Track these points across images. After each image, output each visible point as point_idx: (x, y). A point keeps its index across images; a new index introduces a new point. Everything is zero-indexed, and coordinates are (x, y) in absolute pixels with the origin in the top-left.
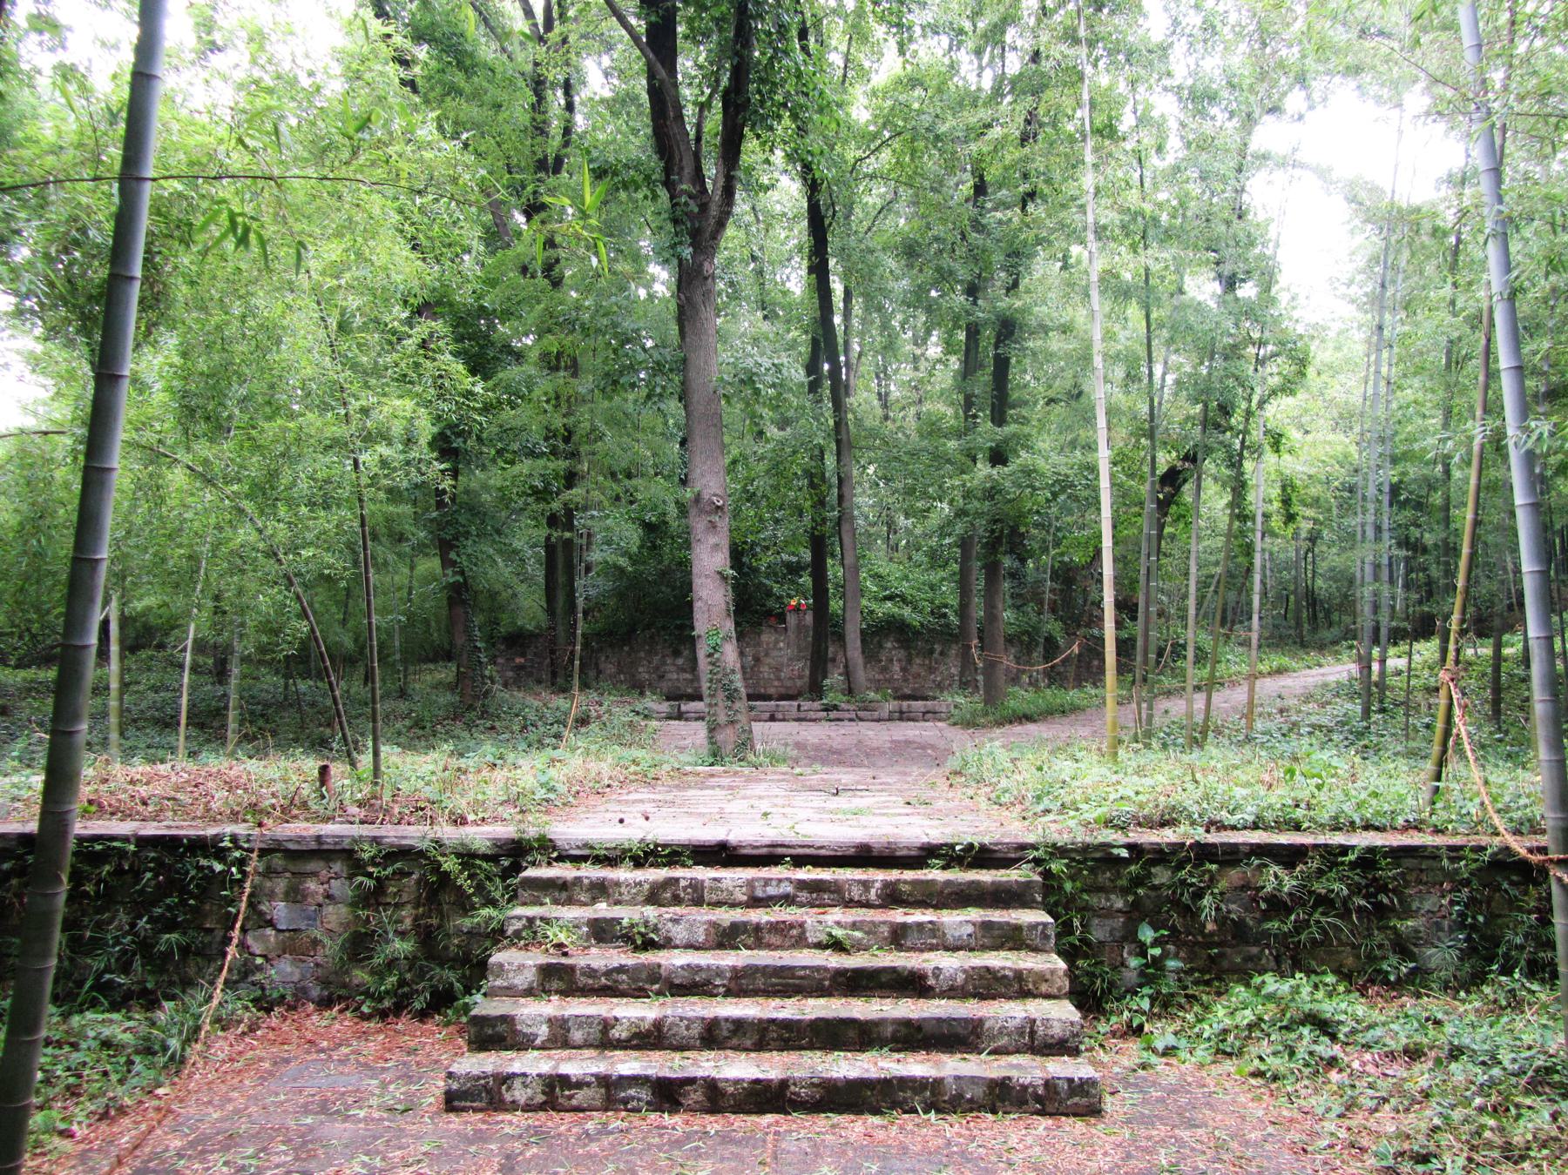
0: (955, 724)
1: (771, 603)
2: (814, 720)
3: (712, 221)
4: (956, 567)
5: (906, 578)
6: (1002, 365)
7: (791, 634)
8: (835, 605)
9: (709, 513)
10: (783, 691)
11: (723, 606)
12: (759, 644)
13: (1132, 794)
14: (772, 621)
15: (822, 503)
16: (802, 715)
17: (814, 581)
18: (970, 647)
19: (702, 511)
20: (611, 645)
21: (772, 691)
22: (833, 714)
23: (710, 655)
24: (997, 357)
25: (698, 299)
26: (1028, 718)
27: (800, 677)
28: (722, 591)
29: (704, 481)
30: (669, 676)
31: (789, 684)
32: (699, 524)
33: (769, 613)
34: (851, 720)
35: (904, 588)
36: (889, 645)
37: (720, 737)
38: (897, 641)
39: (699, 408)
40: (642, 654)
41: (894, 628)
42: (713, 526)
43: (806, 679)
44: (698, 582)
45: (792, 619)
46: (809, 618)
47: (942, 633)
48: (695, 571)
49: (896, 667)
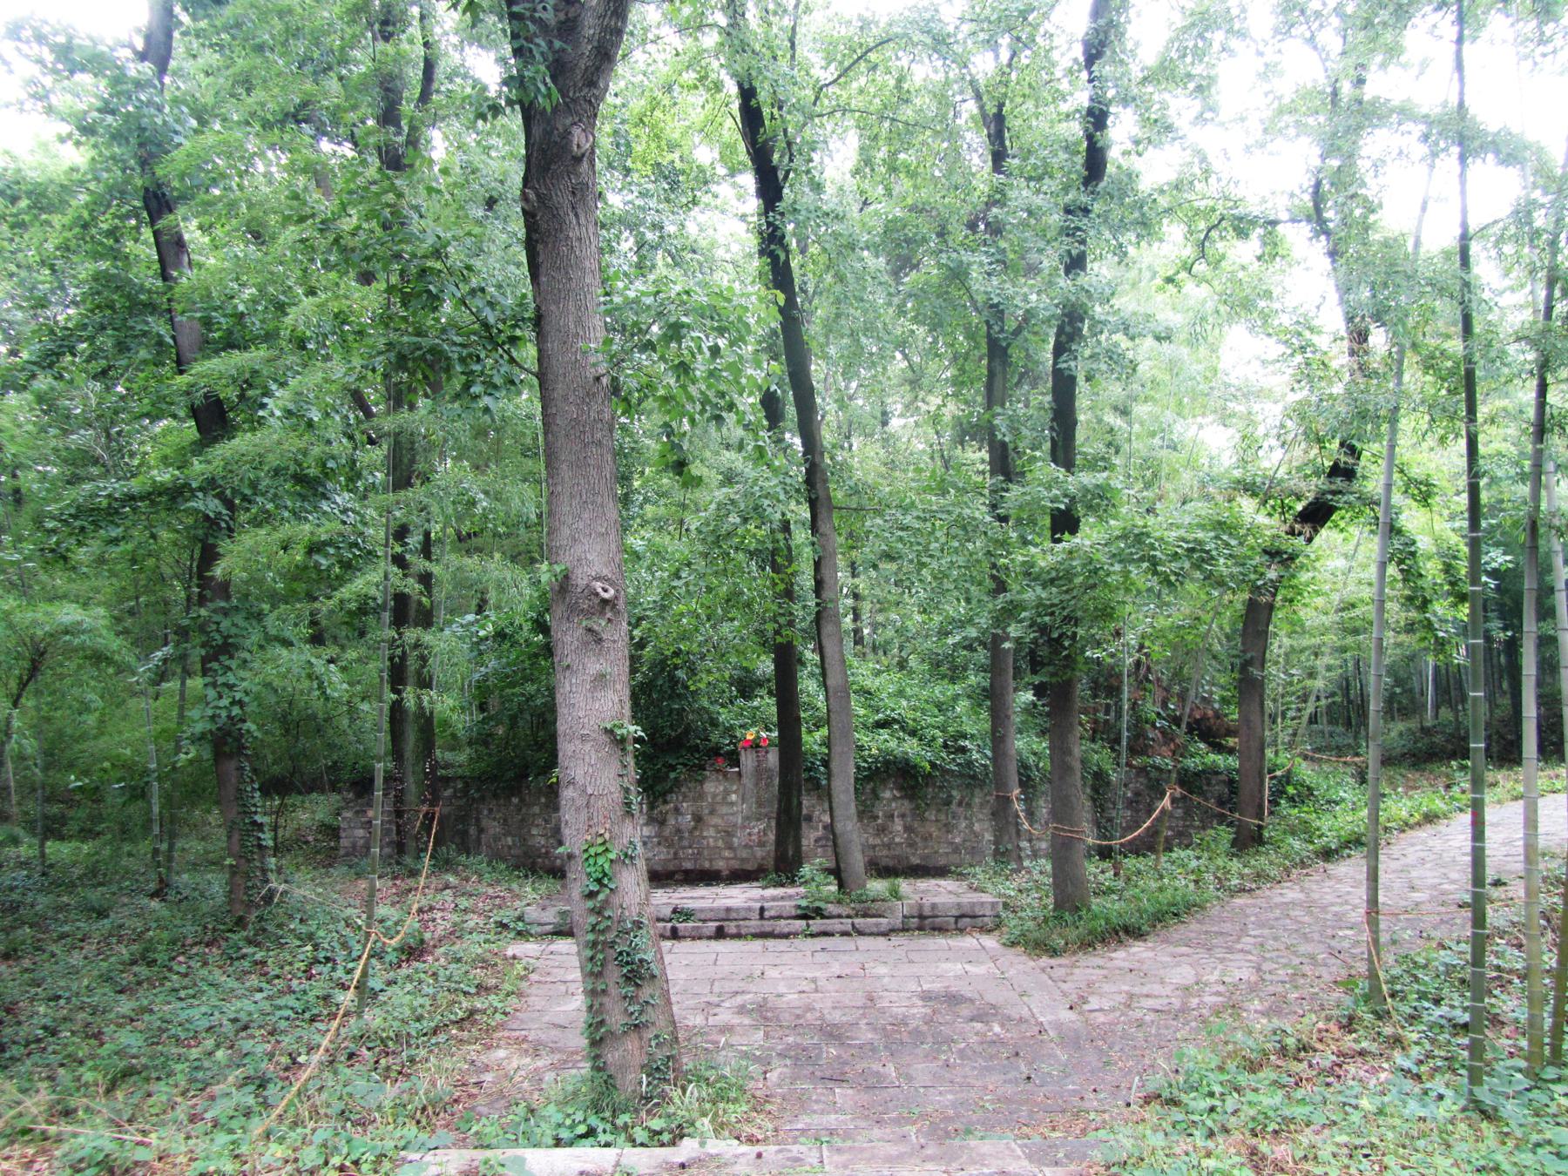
0: (1013, 944)
1: (715, 737)
2: (786, 936)
3: (587, 48)
4: (1365, 812)
5: (900, 693)
6: (1064, 388)
7: (748, 781)
8: (812, 740)
9: (588, 614)
10: (736, 865)
11: (618, 796)
12: (701, 796)
14: (721, 763)
15: (789, 594)
16: (767, 926)
17: (780, 705)
18: (1008, 800)
19: (574, 610)
20: (495, 796)
21: (720, 865)
22: (817, 924)
23: (591, 895)
24: (1057, 373)
25: (562, 198)
26: (1130, 932)
27: (761, 844)
28: (615, 767)
29: (578, 550)
31: (744, 854)
32: (568, 637)
33: (715, 752)
34: (845, 934)
35: (902, 708)
36: (887, 794)
37: (612, 1056)
38: (901, 789)
39: (568, 411)
40: (536, 809)
41: (901, 773)
42: (595, 637)
43: (771, 847)
44: (566, 748)
45: (748, 760)
46: (773, 758)
47: (961, 775)
48: (562, 727)
49: (898, 826)
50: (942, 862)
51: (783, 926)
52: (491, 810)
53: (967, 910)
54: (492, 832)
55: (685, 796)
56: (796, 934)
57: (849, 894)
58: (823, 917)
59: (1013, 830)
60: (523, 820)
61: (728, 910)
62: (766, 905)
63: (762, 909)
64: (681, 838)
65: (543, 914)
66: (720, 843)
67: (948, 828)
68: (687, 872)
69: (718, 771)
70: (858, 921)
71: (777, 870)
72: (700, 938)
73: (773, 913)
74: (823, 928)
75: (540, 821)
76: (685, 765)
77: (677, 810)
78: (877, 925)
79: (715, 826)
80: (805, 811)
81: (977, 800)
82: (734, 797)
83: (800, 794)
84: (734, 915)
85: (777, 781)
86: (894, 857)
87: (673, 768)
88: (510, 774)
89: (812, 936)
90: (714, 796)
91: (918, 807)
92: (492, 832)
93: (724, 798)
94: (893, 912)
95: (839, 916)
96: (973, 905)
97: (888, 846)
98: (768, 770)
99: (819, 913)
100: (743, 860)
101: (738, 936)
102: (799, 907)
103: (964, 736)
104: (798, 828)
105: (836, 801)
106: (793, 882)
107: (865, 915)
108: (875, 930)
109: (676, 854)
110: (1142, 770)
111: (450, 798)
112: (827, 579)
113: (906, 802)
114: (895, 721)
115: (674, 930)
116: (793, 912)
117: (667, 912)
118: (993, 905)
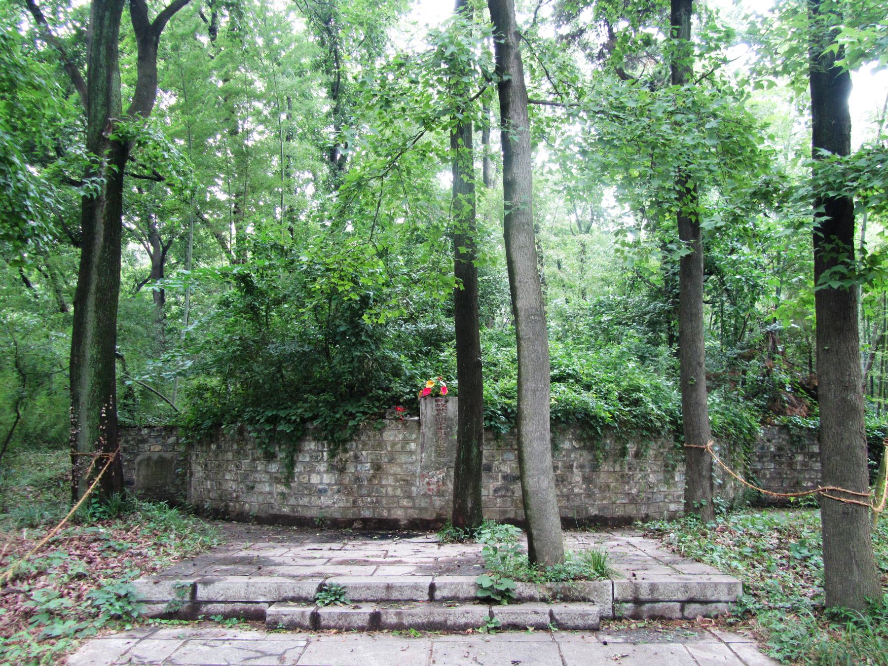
1: (397, 386)
7: (427, 431)
10: (414, 514)
12: (380, 445)
14: (400, 412)
16: (439, 613)
21: (398, 514)
22: (504, 612)
27: (440, 494)
31: (423, 503)
33: (395, 401)
34: (540, 627)
38: (580, 439)
40: (230, 456)
45: (428, 409)
46: (452, 407)
47: (637, 426)
50: (619, 512)
51: (460, 613)
53: (696, 593)
55: (364, 444)
56: (475, 627)
57: (542, 569)
58: (512, 601)
59: (706, 484)
60: (219, 466)
61: (389, 587)
62: (439, 581)
63: (432, 588)
65: (156, 589)
66: (399, 492)
67: (624, 478)
68: (365, 521)
69: (397, 419)
70: (559, 608)
71: (455, 524)
72: (348, 629)
73: (446, 593)
74: (511, 619)
75: (232, 467)
76: (364, 413)
77: (356, 457)
78: (583, 615)
79: (394, 475)
80: (484, 461)
81: (651, 452)
82: (413, 446)
83: (479, 444)
84: (395, 595)
85: (515, 9)
86: (572, 508)
87: (352, 416)
88: (208, 423)
89: (497, 629)
90: (394, 444)
91: (596, 459)
93: (403, 447)
94: (600, 594)
95: (532, 599)
96: (703, 586)
99: (507, 597)
100: (421, 509)
101: (399, 628)
102: (480, 587)
103: (638, 389)
104: (478, 478)
105: (527, 451)
106: (472, 537)
107: (566, 599)
108: (580, 622)
109: (354, 502)
110: (784, 428)
112: (519, 180)
113: (585, 453)
114: (569, 375)
115: (315, 617)
116: (472, 593)
117: (310, 588)
118: (730, 587)
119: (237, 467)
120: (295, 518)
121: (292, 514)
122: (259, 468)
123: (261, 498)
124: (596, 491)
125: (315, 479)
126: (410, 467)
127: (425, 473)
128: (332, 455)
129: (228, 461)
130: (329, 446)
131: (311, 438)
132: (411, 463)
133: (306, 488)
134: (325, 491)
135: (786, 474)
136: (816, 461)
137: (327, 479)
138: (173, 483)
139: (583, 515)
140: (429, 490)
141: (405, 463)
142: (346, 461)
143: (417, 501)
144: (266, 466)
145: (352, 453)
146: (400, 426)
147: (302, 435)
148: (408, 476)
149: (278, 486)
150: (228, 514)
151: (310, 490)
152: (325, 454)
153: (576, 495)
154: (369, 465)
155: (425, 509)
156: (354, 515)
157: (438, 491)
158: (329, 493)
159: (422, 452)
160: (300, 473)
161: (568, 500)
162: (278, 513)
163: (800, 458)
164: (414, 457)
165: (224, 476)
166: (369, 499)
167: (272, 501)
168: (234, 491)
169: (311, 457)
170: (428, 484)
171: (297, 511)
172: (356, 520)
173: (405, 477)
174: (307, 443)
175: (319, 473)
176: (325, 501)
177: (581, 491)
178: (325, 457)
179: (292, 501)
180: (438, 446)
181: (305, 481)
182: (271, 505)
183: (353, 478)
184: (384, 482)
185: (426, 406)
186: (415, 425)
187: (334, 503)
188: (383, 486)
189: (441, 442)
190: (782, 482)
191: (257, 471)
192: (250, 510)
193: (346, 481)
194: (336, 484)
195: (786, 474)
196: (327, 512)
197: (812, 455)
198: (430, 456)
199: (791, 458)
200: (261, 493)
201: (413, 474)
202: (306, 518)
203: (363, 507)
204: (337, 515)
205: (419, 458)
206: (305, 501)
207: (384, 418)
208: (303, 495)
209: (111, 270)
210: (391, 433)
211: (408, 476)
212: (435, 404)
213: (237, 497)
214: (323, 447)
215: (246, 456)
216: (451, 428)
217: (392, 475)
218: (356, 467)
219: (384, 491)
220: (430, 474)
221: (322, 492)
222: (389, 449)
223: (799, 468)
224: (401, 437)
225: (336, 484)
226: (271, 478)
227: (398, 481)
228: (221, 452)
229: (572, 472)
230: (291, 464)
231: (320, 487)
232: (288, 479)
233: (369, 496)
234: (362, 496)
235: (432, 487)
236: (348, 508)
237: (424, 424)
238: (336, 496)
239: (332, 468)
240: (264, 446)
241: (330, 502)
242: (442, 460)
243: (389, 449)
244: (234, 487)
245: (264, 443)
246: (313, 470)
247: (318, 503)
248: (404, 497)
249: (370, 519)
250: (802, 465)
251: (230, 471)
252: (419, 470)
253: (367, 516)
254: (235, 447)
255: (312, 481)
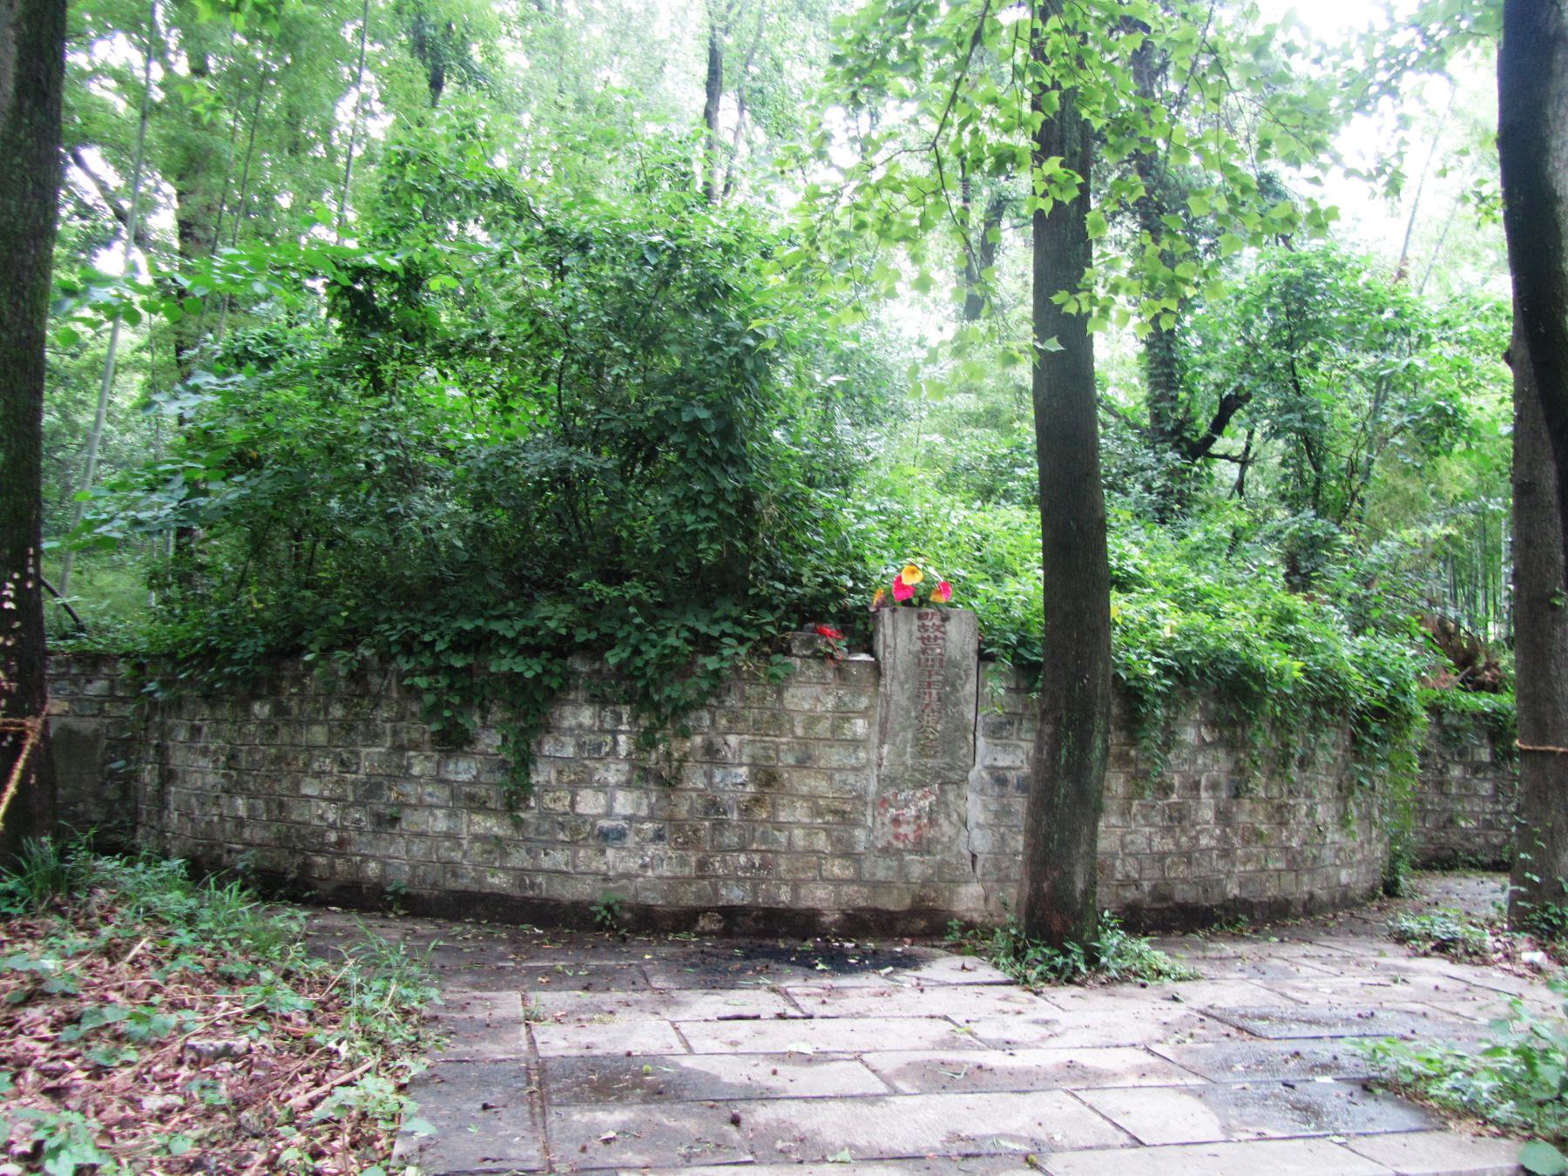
7: (897, 689)
10: (858, 897)
12: (778, 720)
13: (779, 1068)
20: (210, 697)
21: (818, 896)
30: (413, 820)
38: (1212, 724)
40: (319, 734)
52: (195, 731)
54: (196, 780)
64: (719, 826)
66: (821, 842)
68: (730, 913)
77: (711, 752)
79: (811, 798)
82: (860, 726)
87: (708, 645)
90: (812, 721)
92: (196, 780)
93: (835, 729)
97: (1187, 857)
98: (945, 663)
100: (875, 885)
109: (702, 865)
111: (101, 700)
119: (343, 763)
120: (526, 901)
121: (517, 893)
122: (416, 771)
123: (419, 848)
124: (1237, 841)
125: (589, 803)
126: (851, 779)
127: (889, 794)
128: (646, 741)
129: (310, 748)
130: (635, 719)
131: (582, 696)
132: (855, 769)
133: (562, 826)
134: (621, 835)
135: (1432, 803)
136: (1485, 779)
137: (624, 803)
138: (97, 795)
139: (1215, 899)
140: (897, 837)
141: (839, 769)
142: (683, 759)
143: (867, 865)
144: (438, 764)
145: (698, 740)
146: (830, 675)
147: (561, 688)
148: (845, 801)
149: (477, 818)
150: (309, 887)
151: (576, 831)
152: (622, 738)
153: (1202, 851)
154: (744, 771)
155: (887, 884)
156: (698, 896)
157: (919, 838)
158: (631, 840)
159: (881, 743)
160: (547, 787)
161: (1189, 863)
162: (474, 888)
163: (1456, 772)
164: (862, 755)
165: (296, 785)
166: (743, 859)
167: (457, 856)
168: (332, 826)
169: (580, 746)
170: (896, 821)
171: (533, 885)
172: (705, 911)
173: (837, 805)
174: (568, 710)
175: (602, 787)
176: (613, 858)
177: (1213, 843)
178: (623, 749)
179: (519, 859)
180: (921, 730)
181: (563, 805)
182: (451, 867)
183: (699, 804)
184: (783, 816)
185: (895, 628)
186: (867, 675)
187: (644, 866)
188: (780, 827)
189: (929, 718)
190: (1424, 820)
191: (409, 778)
192: (383, 875)
193: (683, 810)
194: (651, 818)
195: (1432, 803)
196: (624, 888)
197: (1477, 768)
198: (901, 754)
199: (1441, 773)
200: (422, 835)
201: (859, 797)
202: (558, 904)
203: (726, 878)
204: (652, 898)
205: (874, 757)
206: (558, 858)
207: (787, 652)
208: (555, 843)
209: (37, 183)
210: (800, 692)
211: (845, 801)
212: (916, 623)
213: (341, 843)
214: (618, 719)
215: (373, 737)
216: (953, 685)
217: (804, 798)
218: (709, 776)
219: (782, 837)
220: (902, 796)
221: (608, 837)
222: (799, 731)
223: (1454, 791)
224: (830, 702)
225: (651, 818)
226: (453, 796)
227: (819, 814)
228: (288, 723)
229: (1198, 798)
230: (526, 761)
231: (605, 824)
232: (515, 800)
233: (743, 849)
234: (728, 850)
235: (903, 830)
236: (687, 881)
237: (889, 673)
238: (651, 850)
239: (642, 776)
240: (447, 713)
241: (633, 864)
242: (930, 763)
243: (799, 731)
244: (331, 817)
245: (449, 705)
246: (584, 780)
247: (598, 864)
248: (833, 855)
249: (743, 908)
250: (1460, 786)
251: (318, 775)
252: (873, 787)
253: (737, 902)
254: (337, 711)
255: (581, 809)
